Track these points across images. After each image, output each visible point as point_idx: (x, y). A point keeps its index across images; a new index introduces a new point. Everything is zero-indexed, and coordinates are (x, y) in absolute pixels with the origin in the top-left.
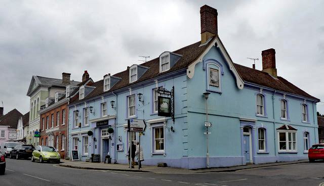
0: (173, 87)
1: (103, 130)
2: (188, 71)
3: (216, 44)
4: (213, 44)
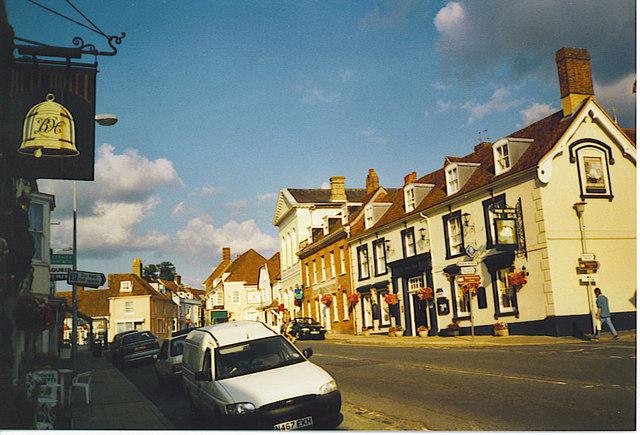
0: (520, 199)
2: (539, 171)
3: (591, 114)
4: (585, 113)
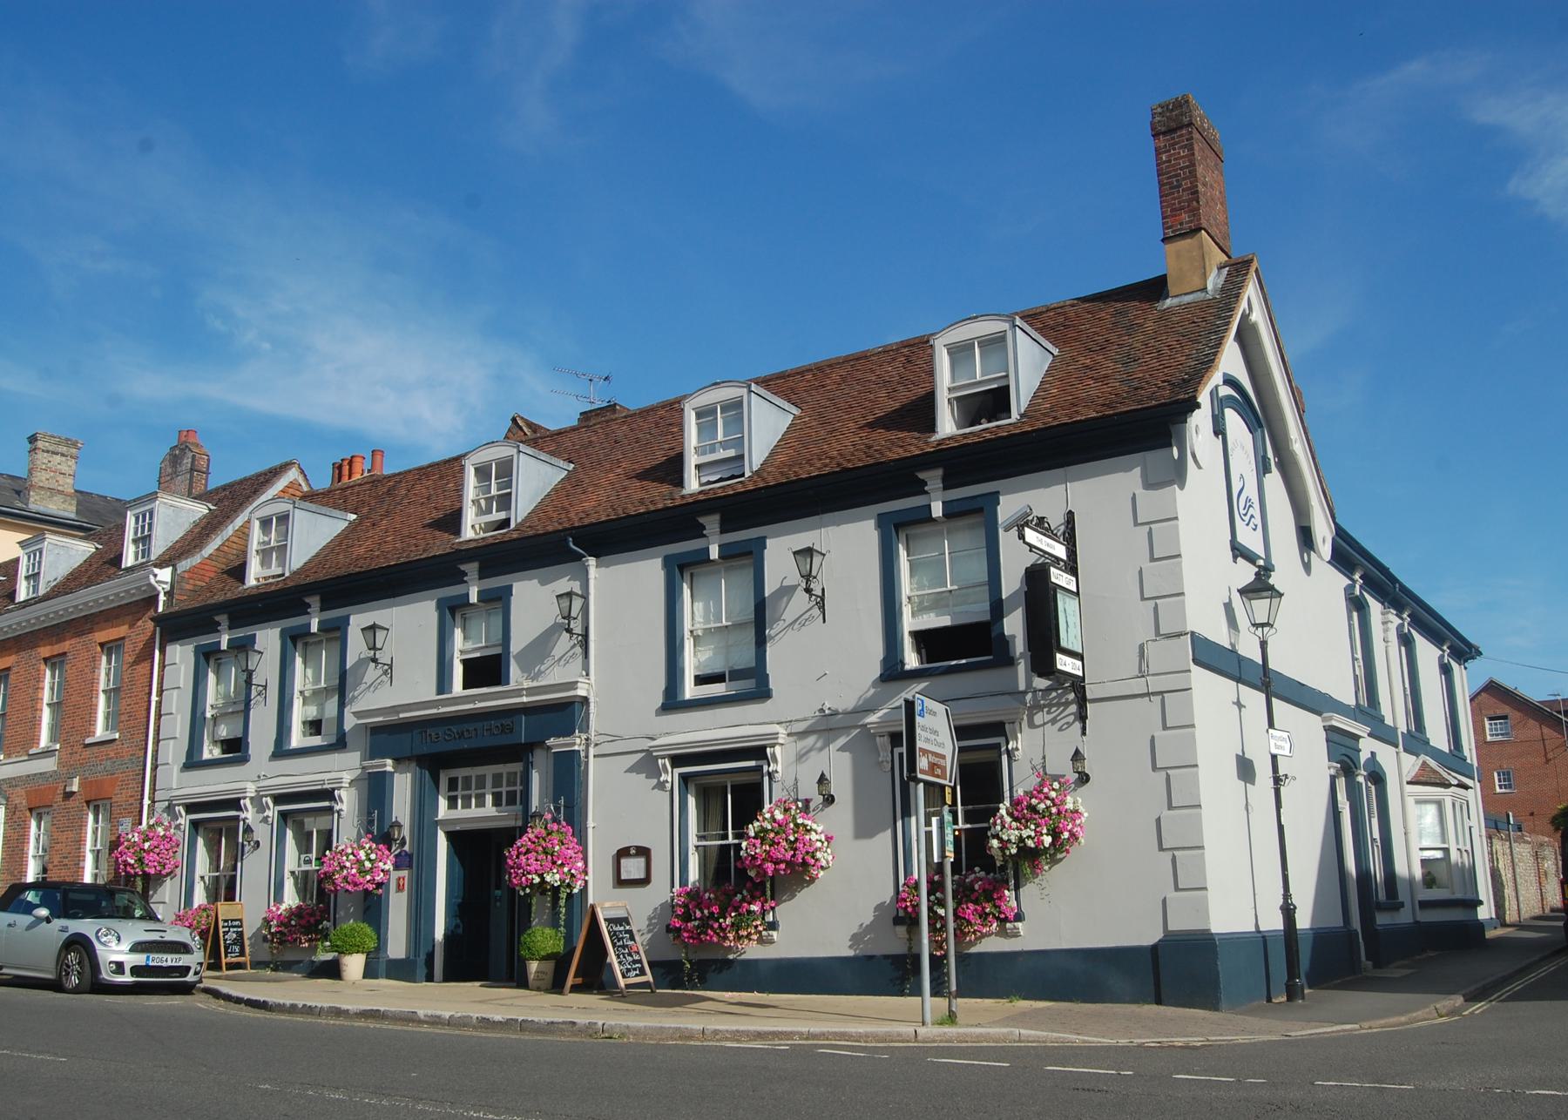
1: (455, 773)
